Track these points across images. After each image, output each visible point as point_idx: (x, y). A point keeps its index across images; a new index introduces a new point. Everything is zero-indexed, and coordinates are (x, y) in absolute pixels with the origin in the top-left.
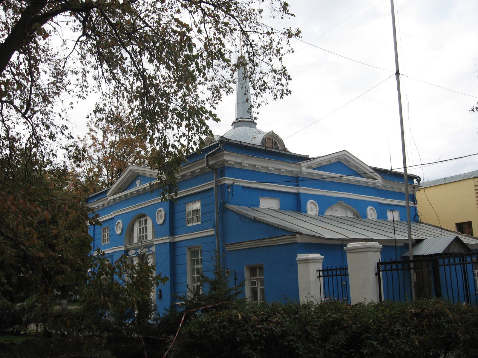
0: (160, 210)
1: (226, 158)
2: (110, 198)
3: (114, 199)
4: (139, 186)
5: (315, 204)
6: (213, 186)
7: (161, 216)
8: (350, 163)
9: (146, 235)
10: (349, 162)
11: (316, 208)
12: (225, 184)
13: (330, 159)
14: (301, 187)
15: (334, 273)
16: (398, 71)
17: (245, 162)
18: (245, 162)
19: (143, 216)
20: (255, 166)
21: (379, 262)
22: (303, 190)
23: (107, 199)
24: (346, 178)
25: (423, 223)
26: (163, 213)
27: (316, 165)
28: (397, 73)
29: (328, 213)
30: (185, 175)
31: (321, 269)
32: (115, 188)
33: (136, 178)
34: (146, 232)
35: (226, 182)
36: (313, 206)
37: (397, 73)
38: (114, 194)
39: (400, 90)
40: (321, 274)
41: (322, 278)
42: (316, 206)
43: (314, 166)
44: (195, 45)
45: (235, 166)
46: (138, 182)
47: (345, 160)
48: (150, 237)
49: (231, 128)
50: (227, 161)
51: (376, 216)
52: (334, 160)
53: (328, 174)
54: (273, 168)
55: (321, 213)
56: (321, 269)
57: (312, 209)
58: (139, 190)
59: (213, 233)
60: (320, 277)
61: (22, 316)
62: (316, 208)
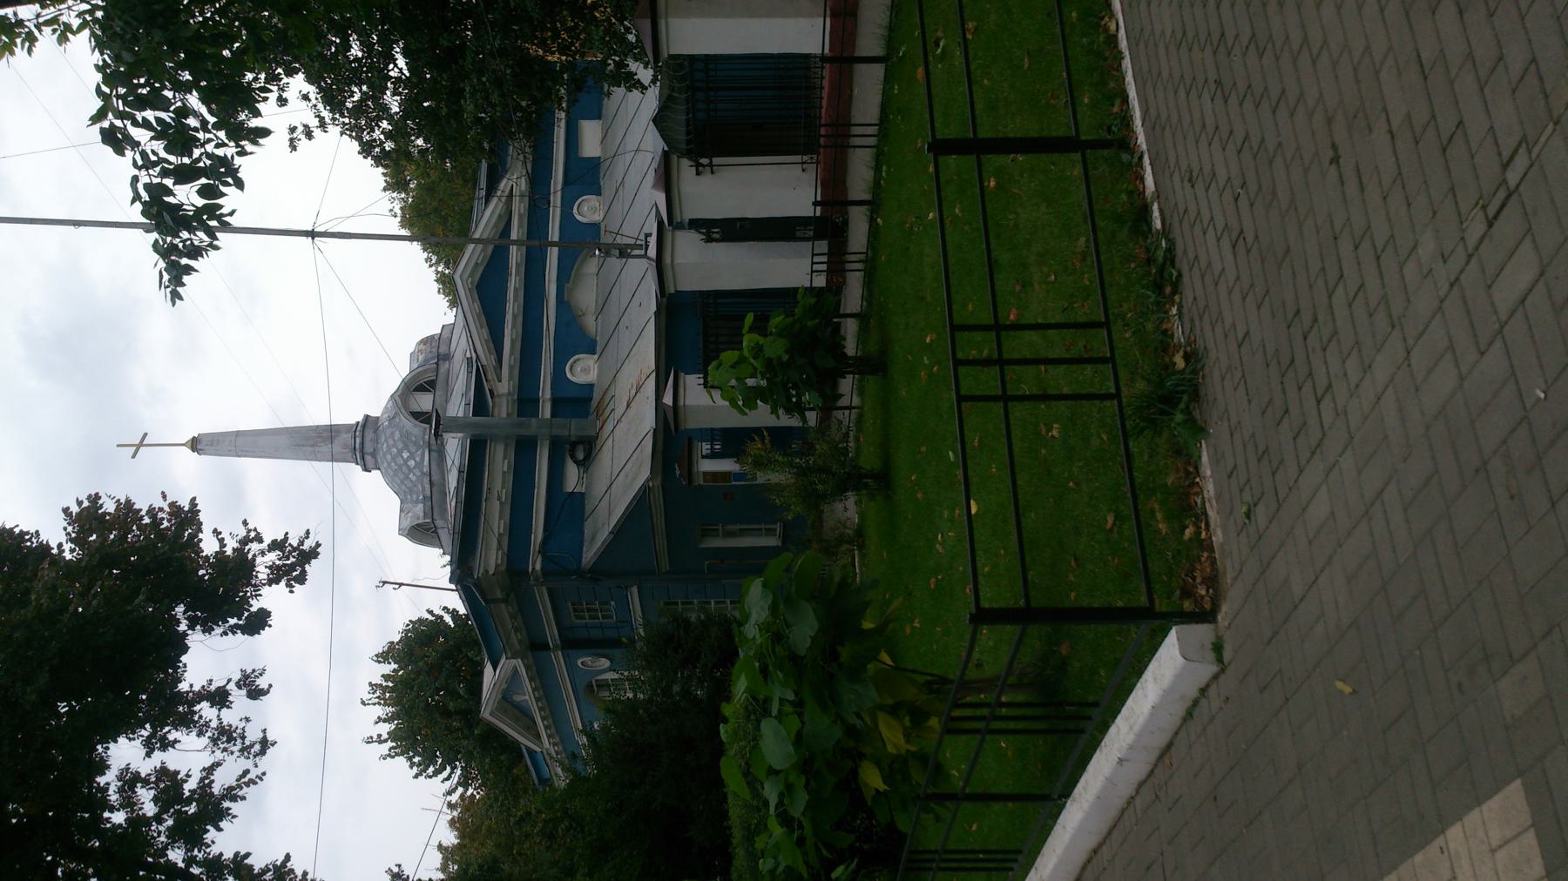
0: (582, 663)
3: (549, 737)
4: (527, 695)
5: (572, 367)
6: (544, 589)
8: (479, 262)
10: (476, 264)
11: (583, 359)
12: (542, 569)
13: (483, 340)
14: (540, 394)
16: (307, 231)
17: (496, 531)
18: (496, 531)
19: (590, 686)
21: (702, 386)
22: (546, 392)
23: (546, 749)
24: (514, 283)
26: (588, 659)
27: (490, 354)
28: (312, 234)
32: (519, 734)
35: (538, 567)
36: (578, 369)
37: (312, 234)
38: (538, 736)
39: (350, 234)
40: (704, 161)
42: (578, 360)
44: (251, 634)
45: (506, 549)
46: (518, 698)
47: (471, 275)
49: (376, 474)
50: (497, 566)
51: (594, 196)
52: (484, 330)
53: (510, 327)
54: (503, 462)
57: (586, 370)
58: (538, 708)
59: (635, 590)
60: (711, 165)
61: (919, 145)
62: (583, 359)
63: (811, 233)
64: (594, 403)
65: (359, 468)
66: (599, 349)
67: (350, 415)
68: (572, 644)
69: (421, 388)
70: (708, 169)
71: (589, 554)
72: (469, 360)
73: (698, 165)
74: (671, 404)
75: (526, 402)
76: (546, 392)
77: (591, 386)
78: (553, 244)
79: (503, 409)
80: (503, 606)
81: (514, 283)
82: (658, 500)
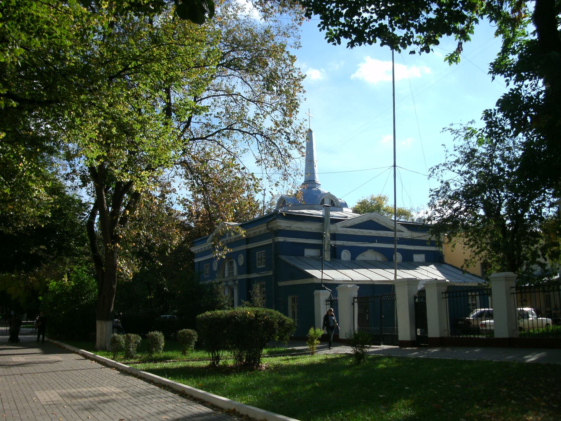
1: (279, 224)
2: (209, 244)
7: (242, 259)
9: (233, 272)
12: (279, 242)
15: (462, 294)
20: (301, 228)
22: (339, 243)
24: (374, 233)
25: (446, 264)
26: (242, 257)
28: (395, 166)
29: (360, 258)
30: (256, 232)
31: (356, 296)
33: (114, 367)
34: (233, 270)
37: (395, 166)
41: (447, 299)
43: (348, 225)
48: (235, 274)
50: (280, 226)
55: (353, 258)
56: (356, 296)
63: (419, 334)
64: (335, 259)
65: (303, 182)
66: (353, 261)
67: (318, 179)
68: (249, 253)
69: (332, 202)
70: (445, 296)
71: (284, 258)
72: (346, 217)
73: (446, 293)
74: (45, 337)
75: (334, 236)
76: (339, 243)
77: (340, 258)
78: (395, 246)
79: (333, 228)
80: (266, 228)
81: (374, 233)
82: (308, 281)
